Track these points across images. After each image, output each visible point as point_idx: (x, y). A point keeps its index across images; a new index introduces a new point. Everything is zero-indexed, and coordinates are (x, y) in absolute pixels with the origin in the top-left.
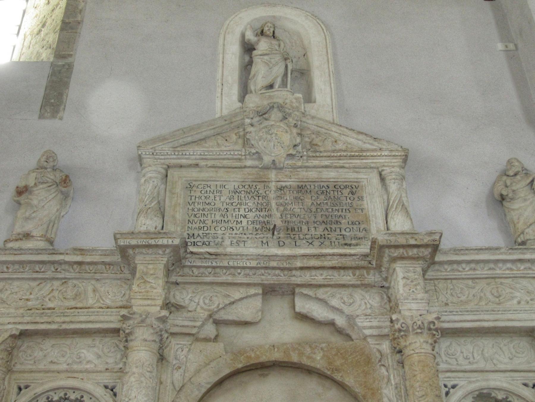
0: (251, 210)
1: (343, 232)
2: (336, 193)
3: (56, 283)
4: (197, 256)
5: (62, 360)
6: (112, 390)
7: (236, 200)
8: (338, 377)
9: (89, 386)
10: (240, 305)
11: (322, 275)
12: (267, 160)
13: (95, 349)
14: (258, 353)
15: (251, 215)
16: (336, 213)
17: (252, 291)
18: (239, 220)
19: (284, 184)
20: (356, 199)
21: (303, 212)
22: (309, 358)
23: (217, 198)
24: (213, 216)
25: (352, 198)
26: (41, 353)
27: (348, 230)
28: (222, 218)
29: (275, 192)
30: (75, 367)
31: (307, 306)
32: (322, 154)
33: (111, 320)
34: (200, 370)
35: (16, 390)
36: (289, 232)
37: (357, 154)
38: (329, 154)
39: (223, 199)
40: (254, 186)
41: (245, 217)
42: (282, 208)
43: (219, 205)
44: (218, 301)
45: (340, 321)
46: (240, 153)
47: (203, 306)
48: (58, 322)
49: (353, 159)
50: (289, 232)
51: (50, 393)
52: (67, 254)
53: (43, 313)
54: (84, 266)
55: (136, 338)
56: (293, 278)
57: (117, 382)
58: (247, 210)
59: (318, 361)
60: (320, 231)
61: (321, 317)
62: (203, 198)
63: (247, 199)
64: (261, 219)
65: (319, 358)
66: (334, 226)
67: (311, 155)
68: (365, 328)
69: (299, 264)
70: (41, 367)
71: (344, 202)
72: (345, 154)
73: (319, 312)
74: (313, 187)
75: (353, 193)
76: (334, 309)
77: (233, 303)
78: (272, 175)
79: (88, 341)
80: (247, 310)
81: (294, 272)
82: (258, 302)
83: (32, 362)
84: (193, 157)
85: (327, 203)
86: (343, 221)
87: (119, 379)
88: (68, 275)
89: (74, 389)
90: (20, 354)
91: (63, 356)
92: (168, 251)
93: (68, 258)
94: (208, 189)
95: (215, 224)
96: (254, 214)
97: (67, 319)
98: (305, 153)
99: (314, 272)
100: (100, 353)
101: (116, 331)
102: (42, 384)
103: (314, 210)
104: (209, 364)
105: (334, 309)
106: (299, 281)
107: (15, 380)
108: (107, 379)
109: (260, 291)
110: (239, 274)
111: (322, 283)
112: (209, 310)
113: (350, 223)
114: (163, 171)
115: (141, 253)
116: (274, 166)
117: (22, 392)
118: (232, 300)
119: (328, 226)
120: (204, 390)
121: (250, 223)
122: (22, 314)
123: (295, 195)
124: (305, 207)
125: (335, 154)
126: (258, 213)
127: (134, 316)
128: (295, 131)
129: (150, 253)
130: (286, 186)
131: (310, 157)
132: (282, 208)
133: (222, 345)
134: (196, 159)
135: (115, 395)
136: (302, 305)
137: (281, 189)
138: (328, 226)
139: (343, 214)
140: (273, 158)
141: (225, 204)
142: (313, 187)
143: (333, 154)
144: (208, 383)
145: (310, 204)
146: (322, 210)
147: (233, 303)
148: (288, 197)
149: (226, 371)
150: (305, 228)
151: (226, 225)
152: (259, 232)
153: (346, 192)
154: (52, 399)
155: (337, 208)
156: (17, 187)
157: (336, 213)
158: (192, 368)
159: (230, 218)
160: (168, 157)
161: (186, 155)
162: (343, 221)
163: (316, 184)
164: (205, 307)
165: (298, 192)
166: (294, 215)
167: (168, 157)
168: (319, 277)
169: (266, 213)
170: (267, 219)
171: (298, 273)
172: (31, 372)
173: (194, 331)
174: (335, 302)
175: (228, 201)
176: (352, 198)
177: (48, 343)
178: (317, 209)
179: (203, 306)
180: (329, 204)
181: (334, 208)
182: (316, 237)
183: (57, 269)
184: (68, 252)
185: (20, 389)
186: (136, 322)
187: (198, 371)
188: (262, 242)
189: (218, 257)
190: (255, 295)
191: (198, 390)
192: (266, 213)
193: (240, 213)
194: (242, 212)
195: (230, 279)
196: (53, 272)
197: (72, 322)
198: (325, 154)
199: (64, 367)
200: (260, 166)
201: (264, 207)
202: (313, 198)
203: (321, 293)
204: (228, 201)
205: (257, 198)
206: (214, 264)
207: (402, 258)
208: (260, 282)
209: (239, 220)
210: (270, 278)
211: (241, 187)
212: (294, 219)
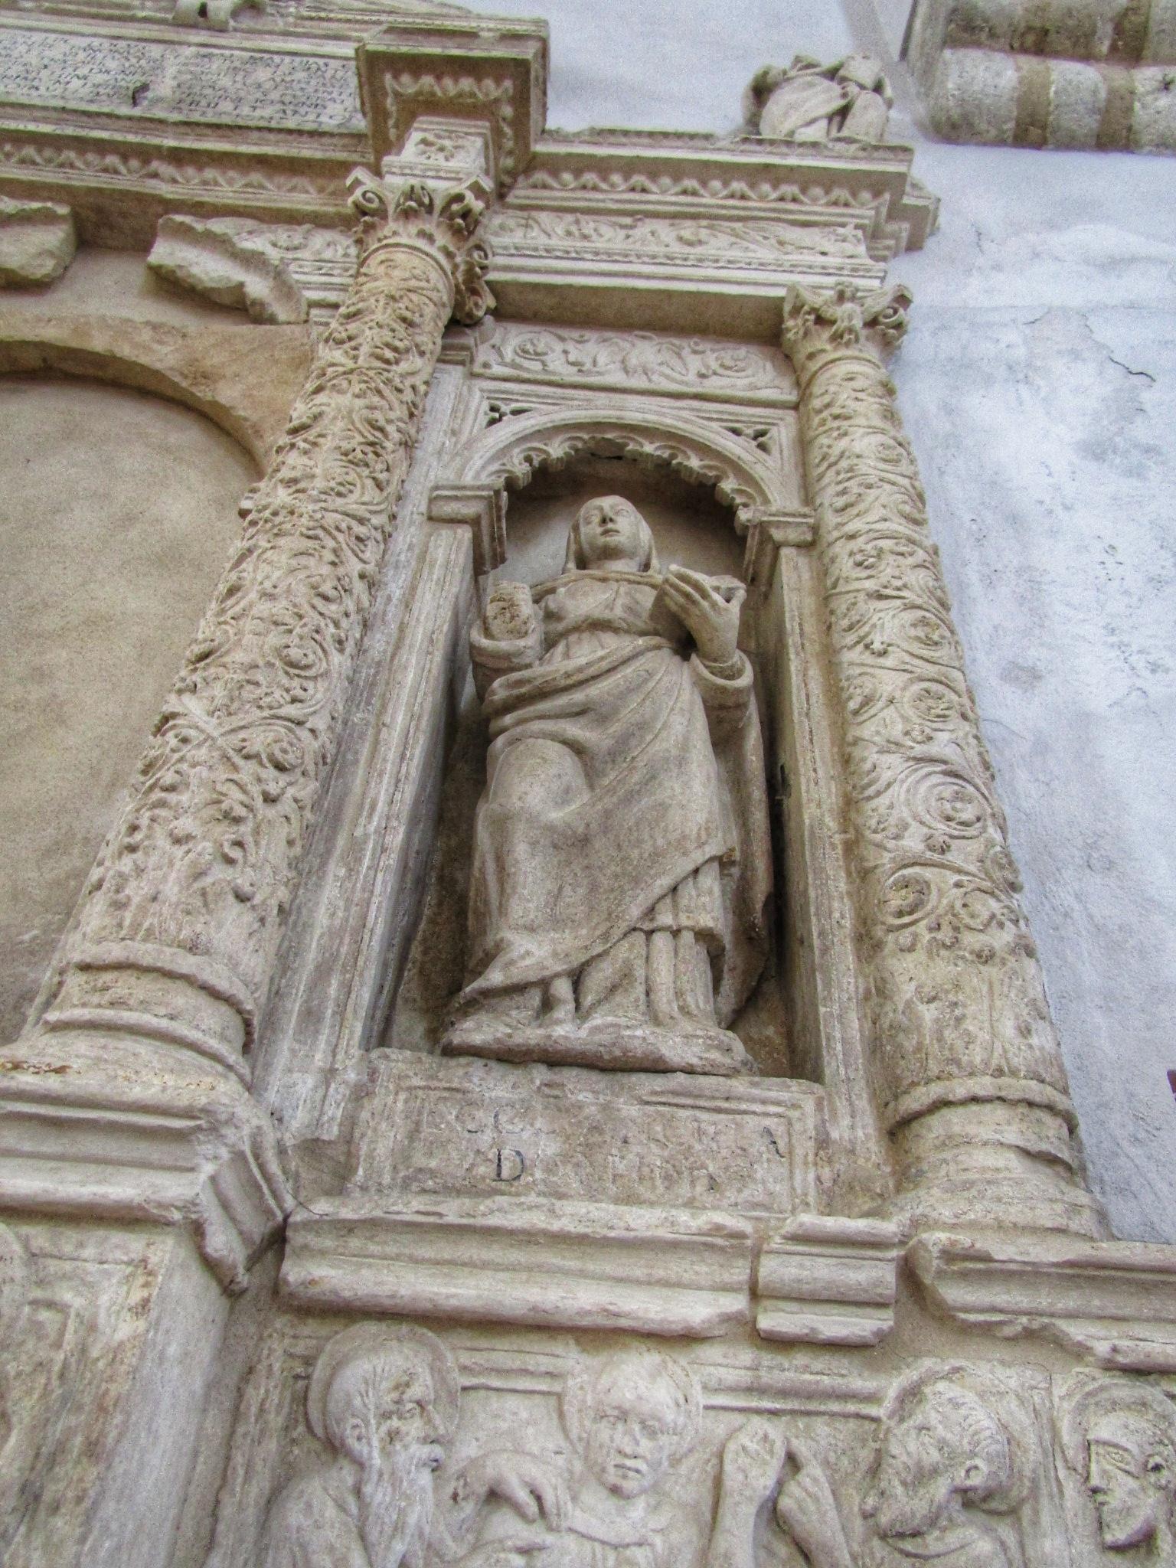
8: (203, 393)
41: (337, 625)
56: (153, 182)
59: (164, 357)
68: (307, 286)
73: (208, 268)
76: (252, 260)
99: (210, 173)
106: (166, 190)
109: (63, 210)
136: (165, 252)
168: (227, 188)
171: (165, 169)
174: (256, 243)
203: (217, 226)
207: (432, 105)
208: (63, 182)
210: (86, 175)
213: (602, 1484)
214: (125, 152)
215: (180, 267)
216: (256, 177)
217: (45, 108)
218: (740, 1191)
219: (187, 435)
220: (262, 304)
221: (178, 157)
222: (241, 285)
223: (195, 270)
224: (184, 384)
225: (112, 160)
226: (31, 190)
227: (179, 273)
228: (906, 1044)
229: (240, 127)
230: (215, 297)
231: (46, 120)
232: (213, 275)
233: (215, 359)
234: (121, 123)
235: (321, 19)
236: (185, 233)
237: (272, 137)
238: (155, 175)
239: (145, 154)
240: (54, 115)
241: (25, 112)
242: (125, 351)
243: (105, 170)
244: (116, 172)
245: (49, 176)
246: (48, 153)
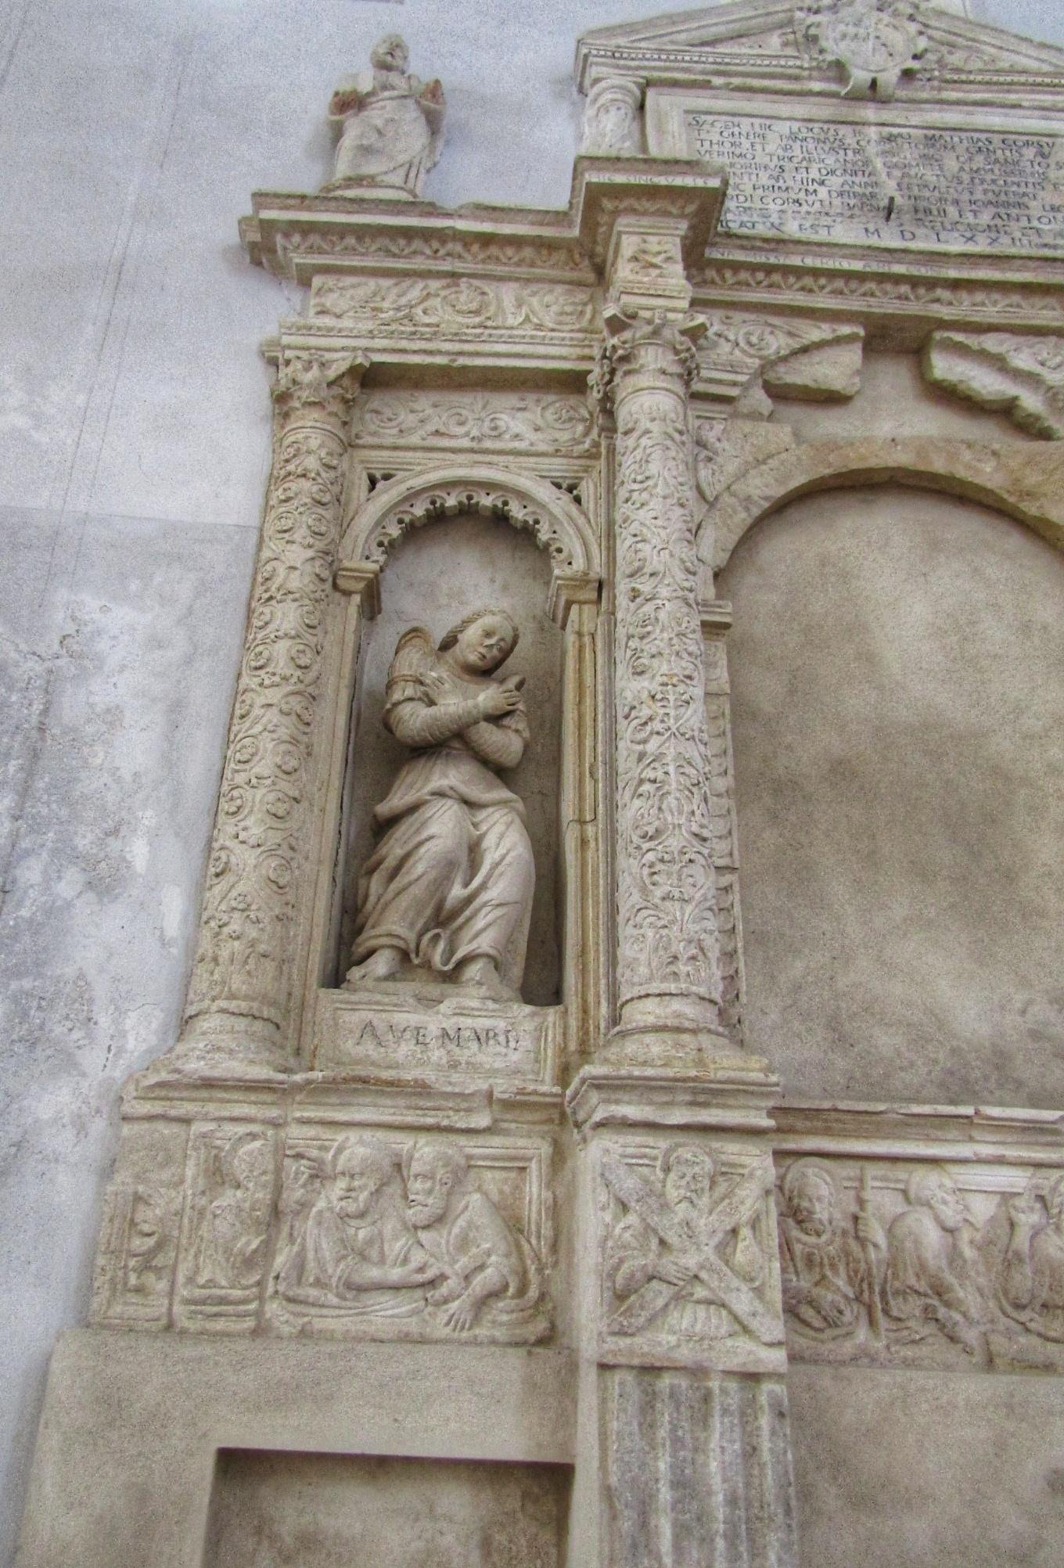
0: (833, 172)
1: (1035, 223)
2: (1008, 153)
3: (434, 285)
4: (739, 242)
5: (461, 430)
6: (570, 489)
7: (797, 152)
8: (1031, 508)
9: (524, 482)
10: (816, 357)
11: (995, 303)
12: (860, 76)
13: (527, 415)
14: (862, 450)
15: (835, 182)
16: (1015, 188)
17: (846, 330)
18: (811, 188)
19: (895, 131)
20: (1053, 166)
21: (943, 183)
22: (968, 467)
23: (758, 147)
24: (754, 177)
25: (1044, 165)
26: (411, 417)
27: (1044, 220)
28: (773, 182)
29: (878, 143)
30: (488, 444)
31: (959, 369)
32: (972, 77)
33: (557, 353)
34: (747, 471)
35: (365, 483)
36: (921, 215)
37: (1047, 80)
38: (987, 78)
39: (770, 148)
40: (832, 132)
42: (897, 173)
43: (761, 158)
44: (777, 344)
45: (1031, 402)
46: (798, 63)
47: (746, 348)
48: (448, 353)
49: (1039, 92)
50: (921, 215)
51: (438, 493)
52: (460, 216)
53: (414, 333)
54: (496, 247)
55: (642, 366)
56: (936, 306)
57: (581, 478)
58: (824, 172)
59: (987, 474)
60: (985, 218)
61: (989, 393)
62: (727, 145)
63: (820, 151)
64: (857, 189)
65: (988, 470)
66: (1014, 212)
67: (948, 77)
69: (953, 273)
70: (414, 440)
71: (1029, 170)
72: (1023, 79)
73: (986, 383)
74: (956, 139)
75: (1043, 155)
76: (1018, 375)
77: (805, 350)
78: (870, 112)
79: (511, 399)
80: (838, 368)
81: (940, 292)
82: (852, 357)
83: (395, 431)
84: (700, 67)
85: (992, 170)
86: (1033, 204)
87: (586, 471)
88: (458, 266)
89: (489, 486)
90: (368, 416)
91: (462, 424)
92: (691, 208)
93: (461, 225)
94: (736, 130)
95: (760, 192)
96: (841, 180)
97: (467, 347)
98: (936, 73)
99: (979, 297)
100: (540, 422)
101: (573, 383)
102: (421, 473)
103: (966, 177)
104: (764, 462)
105: (1018, 375)
106: (945, 312)
107: (362, 462)
108: (558, 466)
110: (822, 288)
111: (996, 321)
112: (761, 358)
113: (1048, 208)
114: (638, 93)
115: (634, 211)
116: (873, 92)
117: (378, 486)
118: (806, 342)
119: (1002, 211)
120: (756, 512)
121: (834, 194)
122: (371, 332)
123: (922, 150)
124: (948, 174)
125: (1002, 79)
126: (848, 177)
127: (634, 322)
128: (913, 28)
129: (652, 209)
130: (900, 135)
131: (947, 81)
132: (897, 173)
133: (788, 429)
134: (703, 72)
135: (578, 500)
136: (944, 366)
137: (890, 138)
138: (1002, 211)
139: (1030, 190)
140: (874, 75)
141: (775, 159)
142: (956, 139)
143: (995, 79)
144: (766, 498)
145: (956, 169)
146: (982, 181)
147: (805, 350)
148: (909, 154)
149: (799, 480)
150: (952, 211)
151: (784, 195)
152: (856, 211)
153: (1029, 153)
154: (442, 505)
155: (1016, 180)
156: (337, 94)
157: (1015, 188)
158: (731, 468)
159: (790, 183)
160: (646, 63)
161: (683, 61)
162: (1033, 204)
163: (964, 135)
164: (752, 351)
165: (926, 146)
166: (926, 186)
167: (646, 63)
168: (992, 309)
169: (866, 179)
170: (870, 189)
172: (396, 448)
173: (734, 392)
174: (1023, 360)
175: (780, 152)
176: (1044, 165)
177: (424, 402)
178: (972, 179)
179: (746, 348)
180: (997, 172)
181: (1009, 180)
182: (980, 228)
183: (436, 251)
184: (463, 211)
185: (373, 482)
186: (638, 335)
187: (742, 475)
188: (867, 230)
189: (781, 246)
190: (850, 339)
191: (747, 509)
192: (866, 179)
193: (811, 176)
194: (814, 174)
195: (801, 300)
196: (428, 257)
197: (478, 354)
198: (979, 78)
199: (465, 443)
200: (843, 93)
201: (864, 167)
202: (962, 159)
203: (991, 343)
204: (780, 152)
205: (842, 152)
206: (772, 260)
208: (865, 309)
209: (811, 188)
210: (886, 304)
211: (804, 130)
212: (927, 194)
213: (129, 1291)
214: (914, 282)
215: (961, 381)
216: (1016, 298)
217: (854, 246)
218: (104, 883)
219: (1014, 541)
220: (1038, 418)
221: (956, 285)
222: (1016, 398)
223: (975, 385)
224: (1012, 500)
225: (904, 289)
226: (835, 316)
227: (961, 387)
228: (122, 615)
229: (1007, 257)
230: (987, 406)
231: (853, 257)
232: (990, 389)
233: (1032, 479)
234: (912, 257)
235: (963, 82)
236: (962, 350)
237: (1031, 264)
238: (938, 300)
239: (932, 284)
240: (860, 252)
241: (835, 250)
242: (962, 473)
243: (899, 298)
244: (907, 299)
245: (855, 304)
246: (854, 284)
